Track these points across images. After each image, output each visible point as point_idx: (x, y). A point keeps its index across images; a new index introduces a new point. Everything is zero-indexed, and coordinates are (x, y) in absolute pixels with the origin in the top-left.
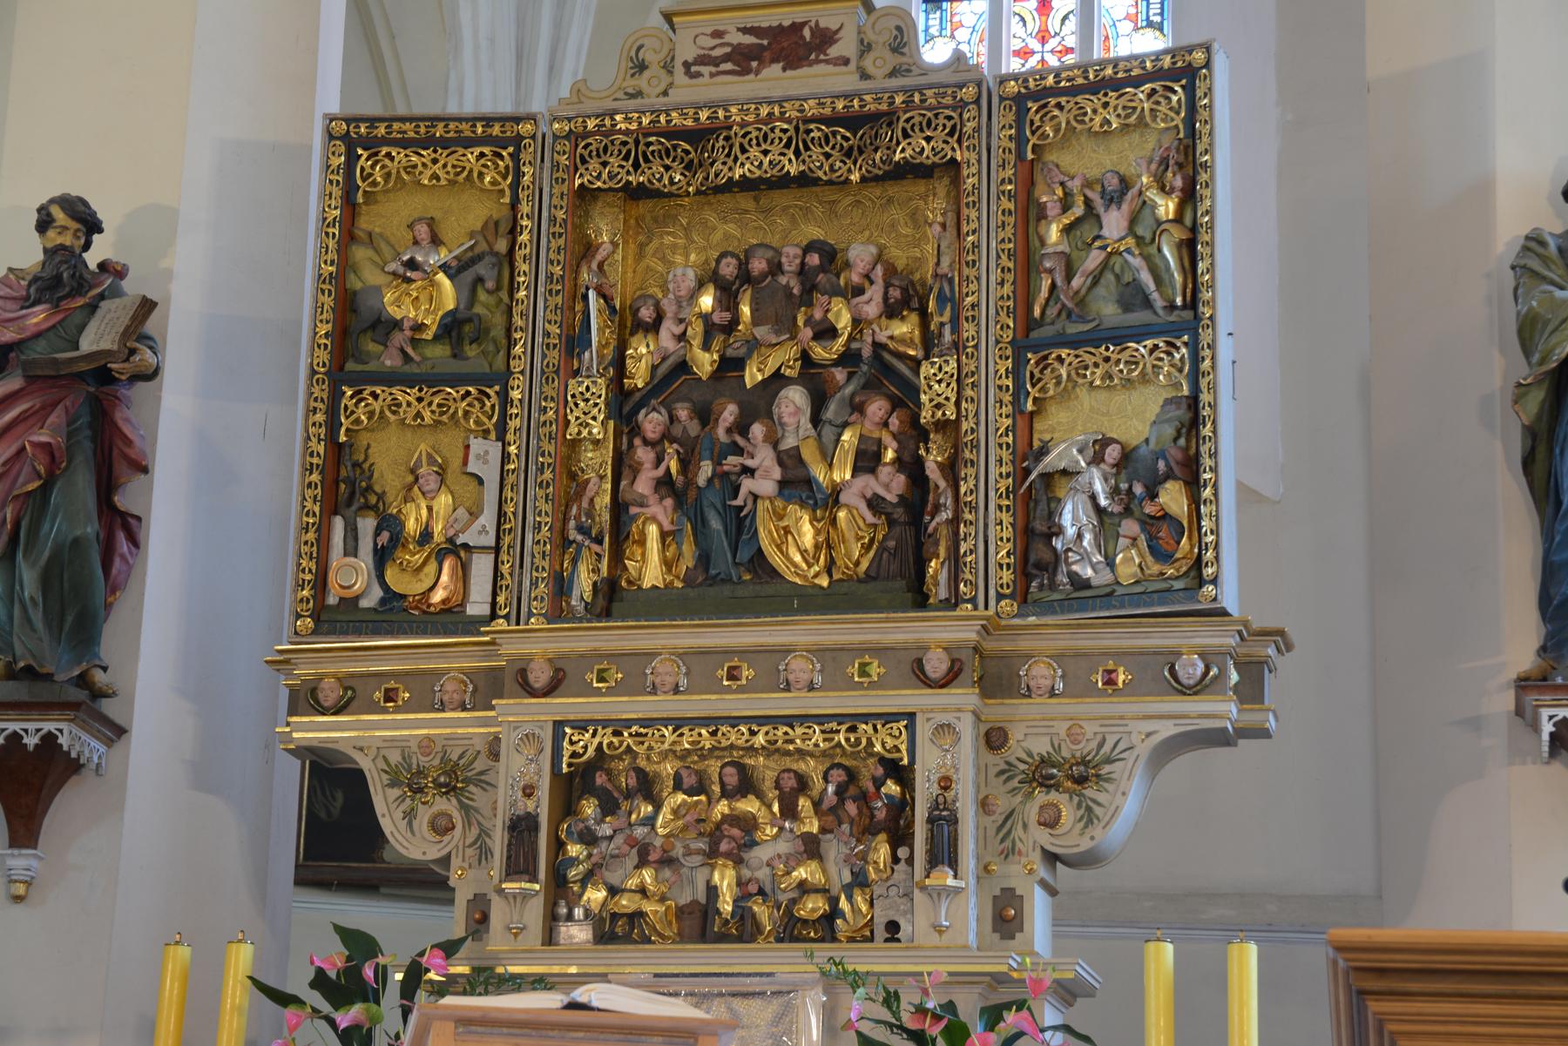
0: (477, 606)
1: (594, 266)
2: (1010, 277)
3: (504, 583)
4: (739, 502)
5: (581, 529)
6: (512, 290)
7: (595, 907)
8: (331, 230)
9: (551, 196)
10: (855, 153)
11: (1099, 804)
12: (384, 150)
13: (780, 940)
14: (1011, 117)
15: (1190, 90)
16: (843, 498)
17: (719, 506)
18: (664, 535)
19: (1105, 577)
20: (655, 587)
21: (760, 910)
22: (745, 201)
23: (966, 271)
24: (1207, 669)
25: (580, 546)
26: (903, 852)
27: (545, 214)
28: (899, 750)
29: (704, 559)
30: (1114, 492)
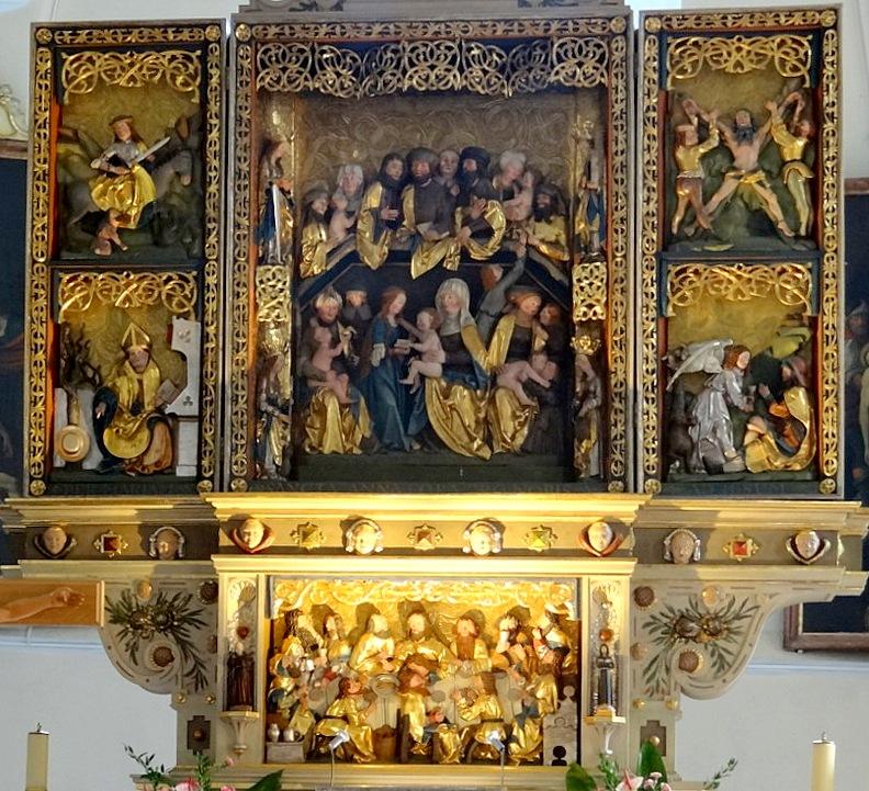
0: (185, 469)
1: (273, 162)
2: (654, 196)
3: (208, 448)
4: (409, 381)
5: (271, 401)
6: (205, 183)
7: (304, 731)
8: (42, 131)
9: (237, 97)
10: (508, 69)
11: (729, 652)
12: (87, 54)
13: (463, 761)
14: (654, 51)
15: (817, 45)
16: (500, 381)
17: (392, 384)
18: (342, 406)
19: (737, 464)
20: (334, 452)
22: (402, 106)
23: (615, 188)
24: (822, 545)
25: (270, 416)
27: (232, 113)
29: (378, 430)
30: (745, 391)
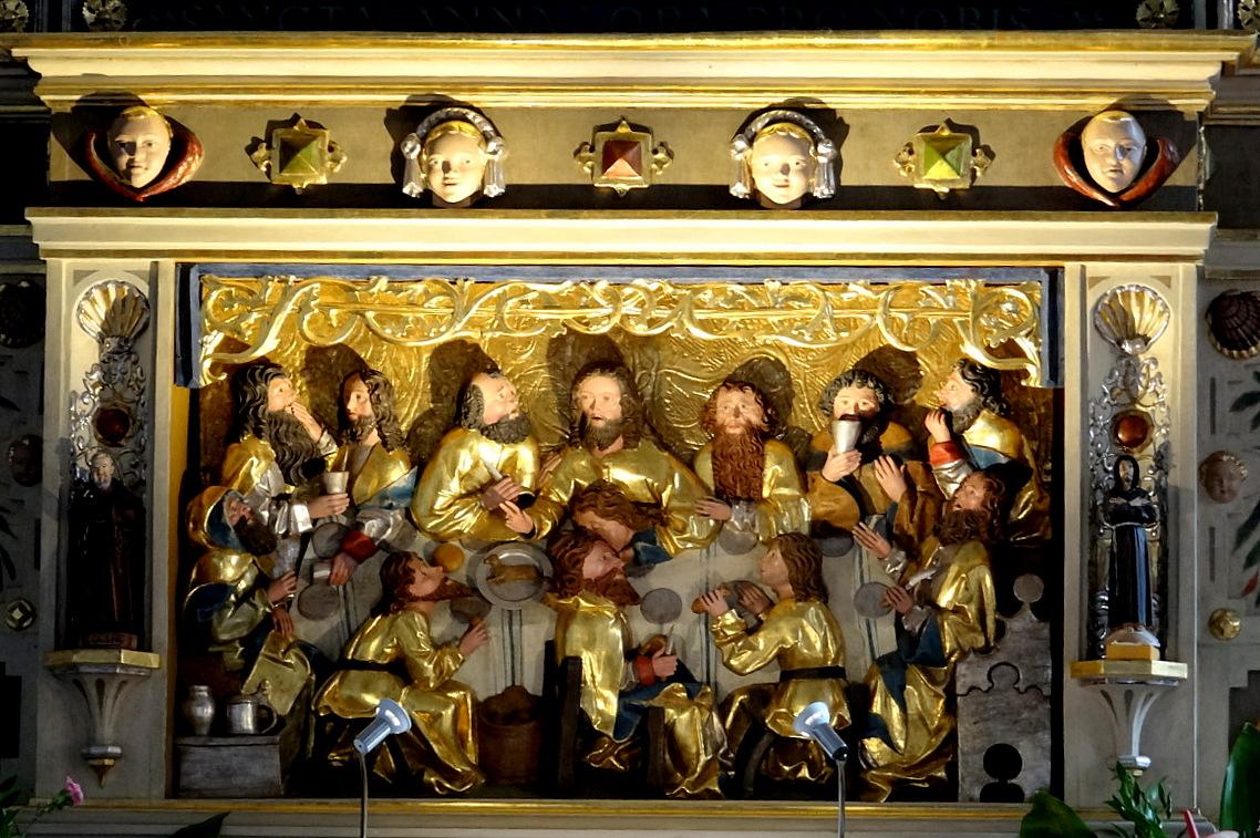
7: (282, 705)
13: (732, 790)
21: (687, 722)
26: (1027, 589)
28: (1019, 353)
